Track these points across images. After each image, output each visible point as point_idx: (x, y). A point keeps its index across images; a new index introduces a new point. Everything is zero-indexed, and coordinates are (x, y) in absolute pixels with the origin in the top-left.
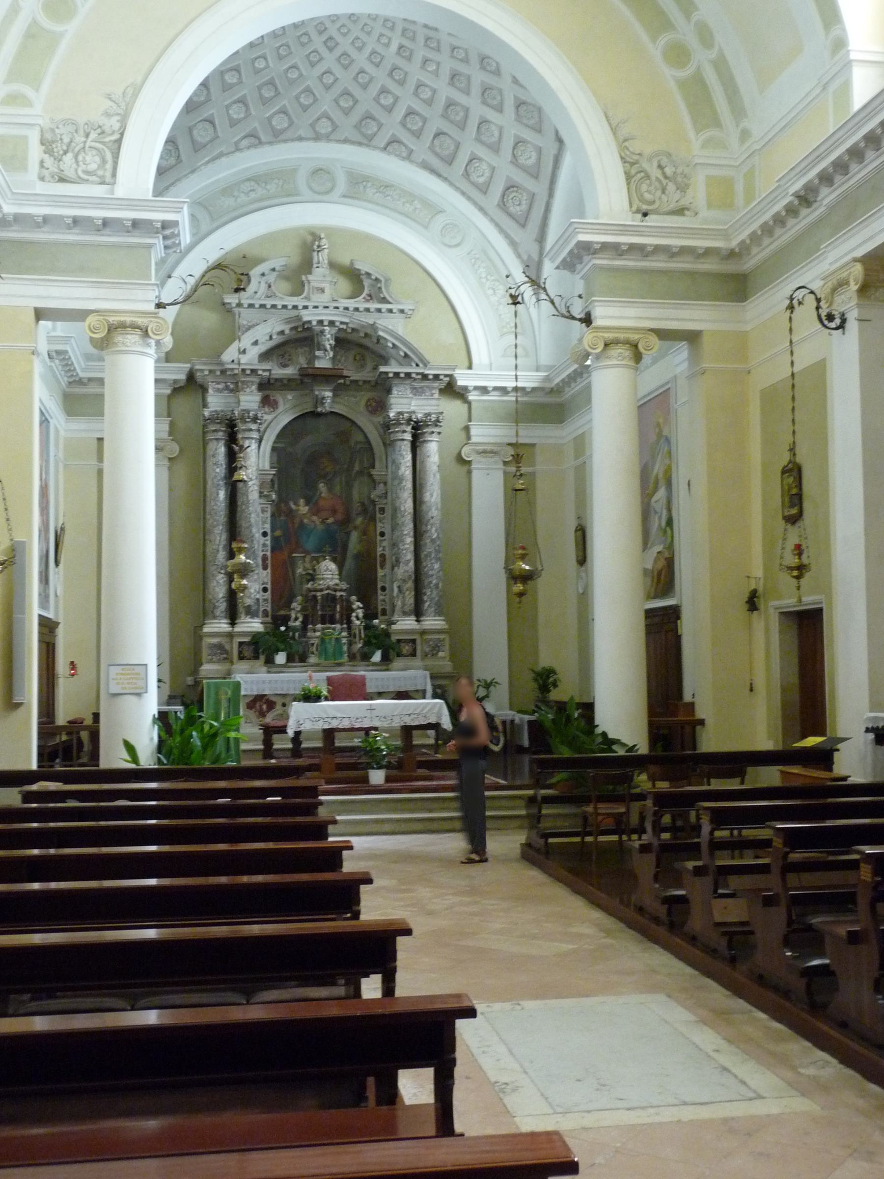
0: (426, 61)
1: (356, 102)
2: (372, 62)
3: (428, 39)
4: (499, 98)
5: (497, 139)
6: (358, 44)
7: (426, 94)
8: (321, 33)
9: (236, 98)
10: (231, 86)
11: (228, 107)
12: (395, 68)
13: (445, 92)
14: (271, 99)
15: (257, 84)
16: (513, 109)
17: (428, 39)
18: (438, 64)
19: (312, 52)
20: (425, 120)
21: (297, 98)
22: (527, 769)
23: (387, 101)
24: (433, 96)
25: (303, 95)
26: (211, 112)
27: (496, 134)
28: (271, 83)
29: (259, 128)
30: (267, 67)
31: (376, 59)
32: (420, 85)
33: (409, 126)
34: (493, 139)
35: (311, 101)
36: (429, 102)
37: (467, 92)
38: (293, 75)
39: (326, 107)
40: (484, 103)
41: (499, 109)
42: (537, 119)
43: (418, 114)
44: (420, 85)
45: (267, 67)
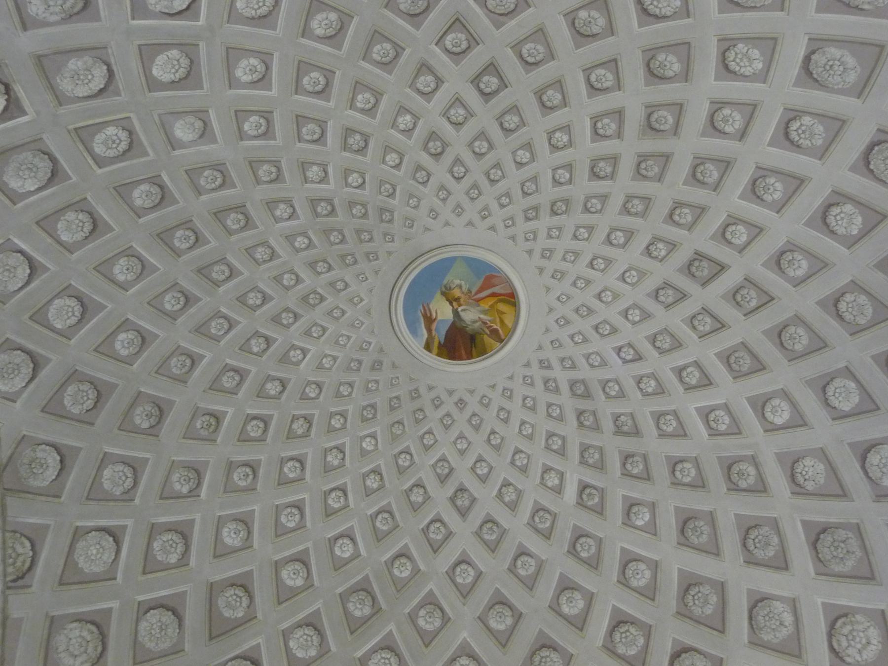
0: (630, 506)
1: (518, 617)
2: (537, 531)
3: (627, 457)
4: (776, 540)
5: (791, 629)
6: (510, 495)
7: (641, 577)
8: (443, 480)
9: (300, 616)
10: (294, 592)
11: (286, 635)
12: (579, 535)
13: (677, 561)
14: (366, 620)
15: (340, 590)
16: (806, 550)
17: (627, 457)
18: (653, 507)
19: (433, 521)
20: (648, 631)
21: (412, 618)
22: (493, 341)
23: (573, 606)
24: (655, 577)
25: (422, 613)
26: (253, 643)
27: (788, 618)
28: (364, 588)
29: (251, 376)
30: (356, 555)
31: (543, 522)
32: (628, 560)
33: (621, 650)
34: (784, 633)
35: (438, 623)
36: (650, 593)
37: (714, 550)
38: (403, 571)
39: (464, 634)
40: (752, 562)
41: (781, 564)
42: (859, 553)
43: (633, 622)
44: (628, 560)
45: (356, 555)
